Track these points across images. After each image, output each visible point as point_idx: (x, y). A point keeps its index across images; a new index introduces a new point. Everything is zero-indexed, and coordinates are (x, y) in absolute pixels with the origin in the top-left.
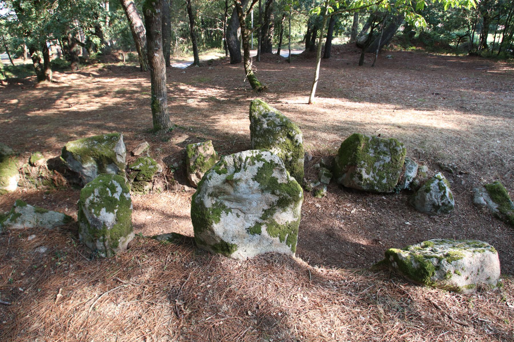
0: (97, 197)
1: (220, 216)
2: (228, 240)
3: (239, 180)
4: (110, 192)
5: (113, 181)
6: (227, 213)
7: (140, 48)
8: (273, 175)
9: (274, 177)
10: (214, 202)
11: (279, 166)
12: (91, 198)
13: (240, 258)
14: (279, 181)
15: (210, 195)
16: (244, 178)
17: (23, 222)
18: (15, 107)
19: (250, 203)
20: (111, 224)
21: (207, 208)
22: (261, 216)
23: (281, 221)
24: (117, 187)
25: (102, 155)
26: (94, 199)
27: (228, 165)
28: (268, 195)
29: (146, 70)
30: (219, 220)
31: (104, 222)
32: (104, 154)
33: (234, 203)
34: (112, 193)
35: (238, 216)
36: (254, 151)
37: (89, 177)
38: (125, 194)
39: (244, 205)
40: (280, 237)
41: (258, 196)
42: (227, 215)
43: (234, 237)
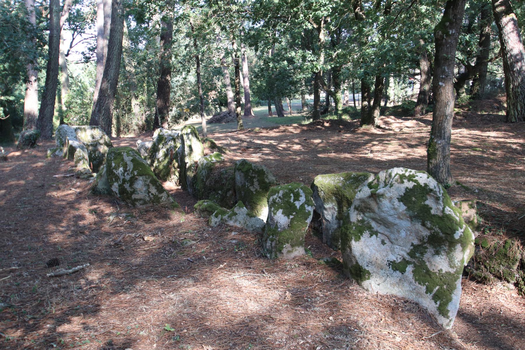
0: (280, 198)
1: (362, 234)
2: (363, 263)
3: (382, 195)
4: (292, 198)
5: (300, 190)
6: (371, 235)
7: (511, 86)
8: (427, 202)
9: (428, 206)
10: (360, 218)
11: (435, 193)
12: (275, 197)
13: (370, 289)
14: (433, 212)
15: (356, 208)
16: (388, 195)
17: (236, 221)
18: (313, 147)
19: (398, 232)
20: (282, 227)
21: (351, 222)
22: (408, 251)
23: (433, 267)
24: (301, 196)
25: (344, 195)
26: (276, 199)
27: (380, 180)
28: (418, 226)
29: (513, 120)
30: (360, 238)
31: (277, 222)
32: (345, 194)
33: (382, 227)
34: (295, 200)
35: (383, 243)
36: (409, 170)
37: (328, 221)
38: (306, 206)
39: (392, 232)
40: (427, 288)
41: (405, 224)
42: (370, 237)
43: (370, 263)
